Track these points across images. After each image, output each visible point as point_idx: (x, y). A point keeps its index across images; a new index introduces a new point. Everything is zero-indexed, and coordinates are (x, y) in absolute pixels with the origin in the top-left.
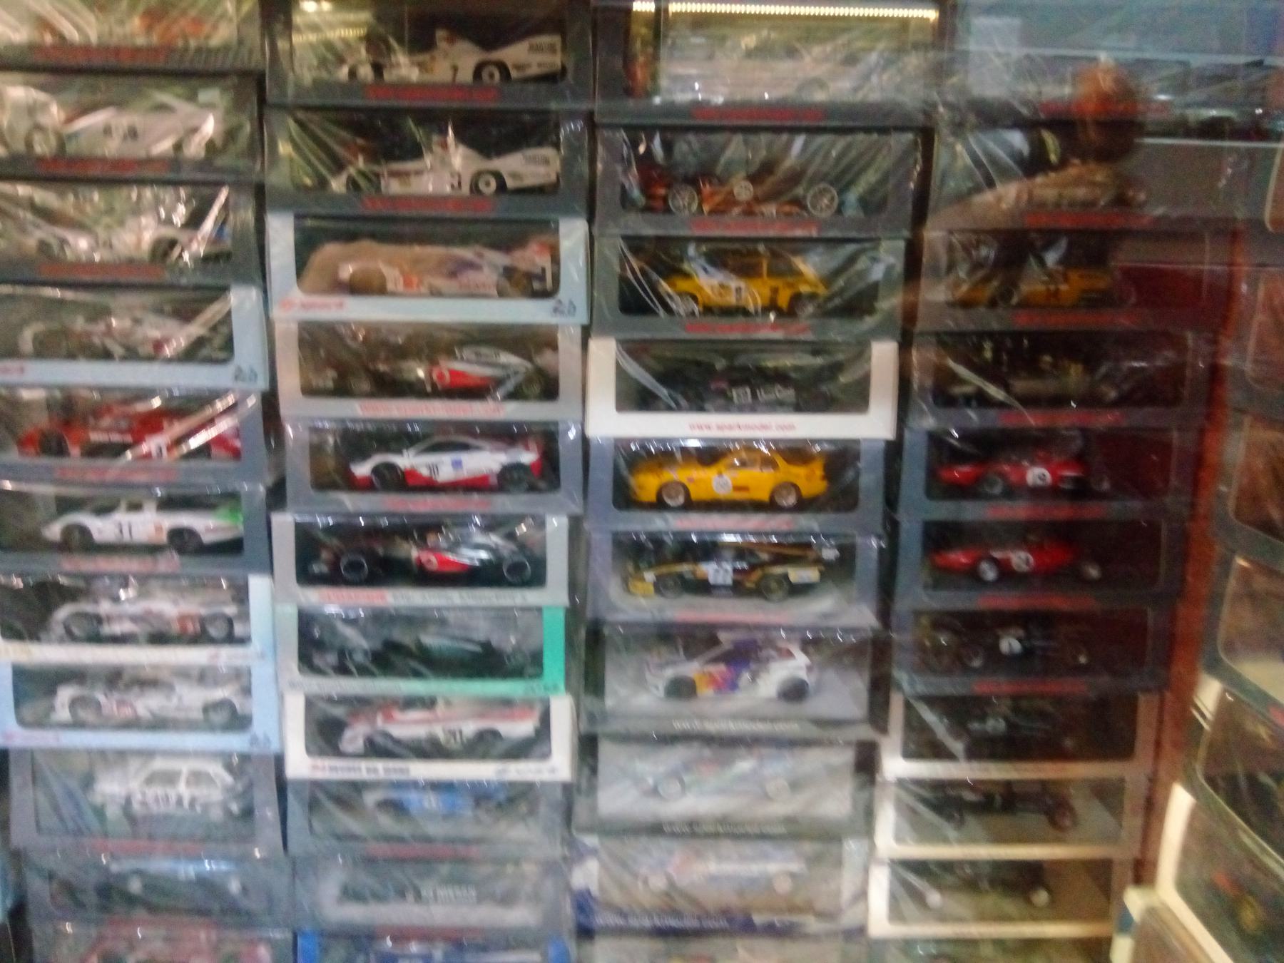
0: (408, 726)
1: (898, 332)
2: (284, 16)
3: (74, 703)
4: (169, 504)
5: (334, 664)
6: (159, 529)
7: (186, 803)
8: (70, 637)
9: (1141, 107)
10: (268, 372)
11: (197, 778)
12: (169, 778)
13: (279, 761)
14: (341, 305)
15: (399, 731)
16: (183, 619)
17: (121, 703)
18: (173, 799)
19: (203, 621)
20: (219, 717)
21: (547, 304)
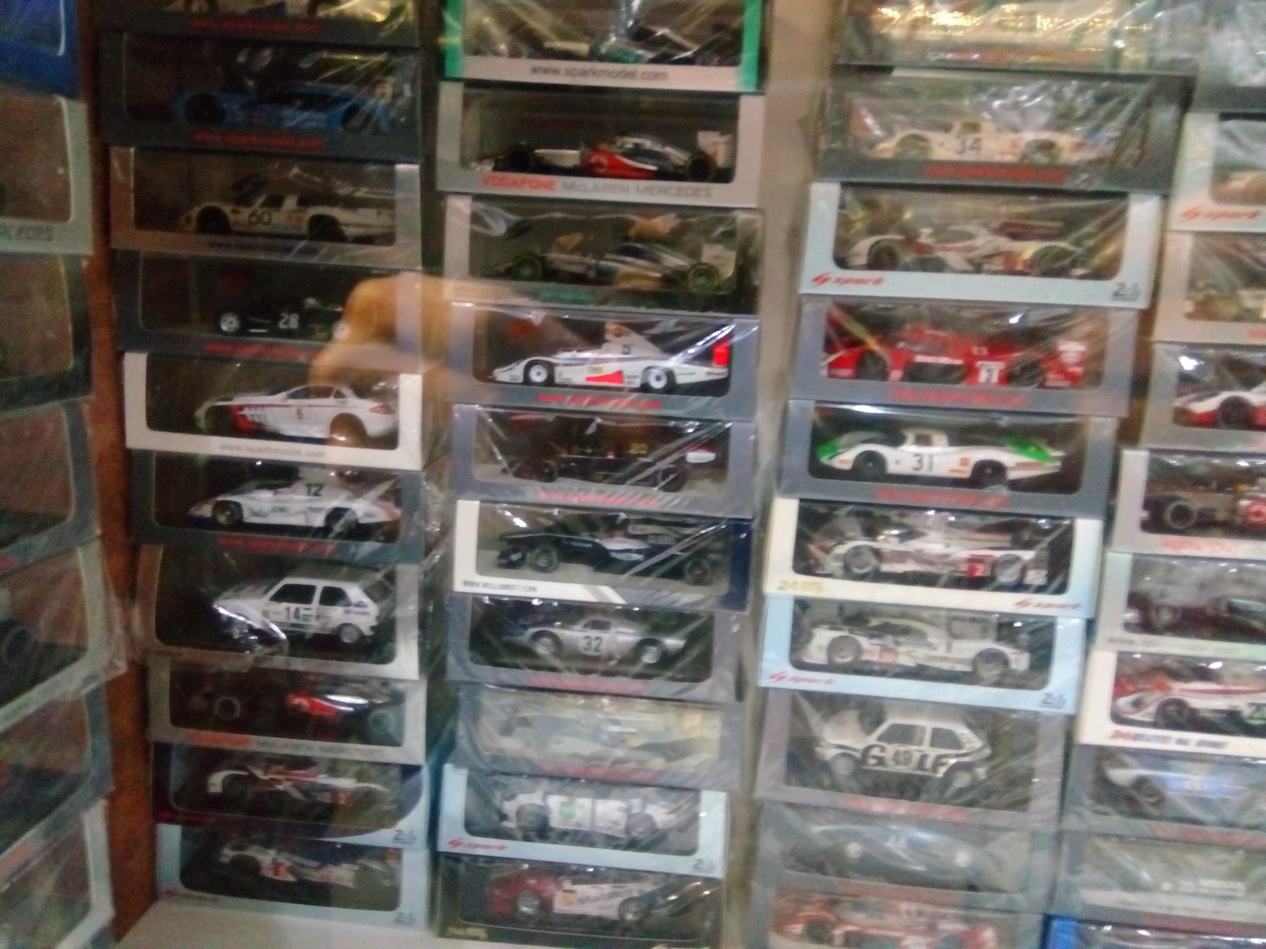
0: (1202, 698)
1: (1197, 376)
2: (599, 49)
3: (833, 646)
4: (963, 436)
5: (1137, 621)
6: (964, 462)
7: (929, 763)
8: (849, 573)
9: (480, 332)
10: (1152, 285)
11: (941, 738)
12: (904, 734)
13: (1071, 724)
14: (878, 282)
15: (1197, 703)
16: (974, 560)
17: (885, 649)
18: (916, 757)
19: (995, 565)
20: (991, 672)
21: (1109, 286)
